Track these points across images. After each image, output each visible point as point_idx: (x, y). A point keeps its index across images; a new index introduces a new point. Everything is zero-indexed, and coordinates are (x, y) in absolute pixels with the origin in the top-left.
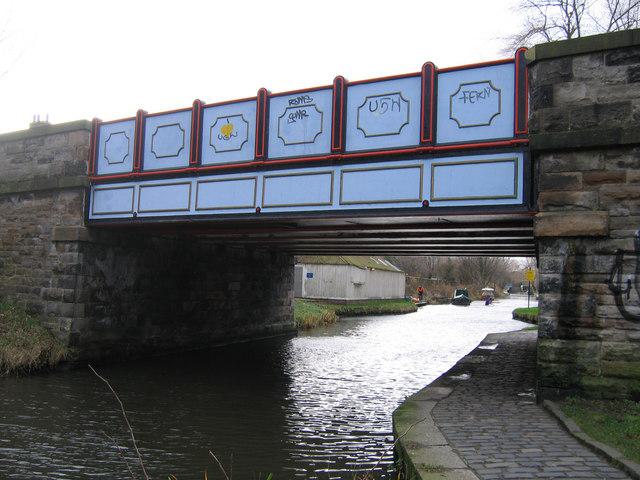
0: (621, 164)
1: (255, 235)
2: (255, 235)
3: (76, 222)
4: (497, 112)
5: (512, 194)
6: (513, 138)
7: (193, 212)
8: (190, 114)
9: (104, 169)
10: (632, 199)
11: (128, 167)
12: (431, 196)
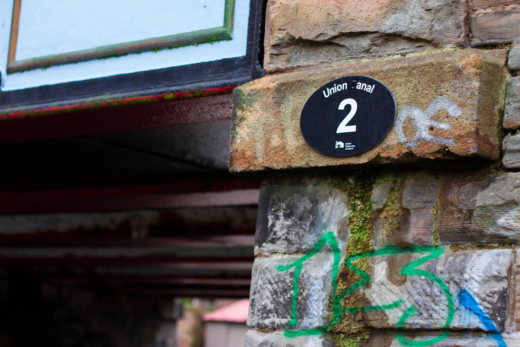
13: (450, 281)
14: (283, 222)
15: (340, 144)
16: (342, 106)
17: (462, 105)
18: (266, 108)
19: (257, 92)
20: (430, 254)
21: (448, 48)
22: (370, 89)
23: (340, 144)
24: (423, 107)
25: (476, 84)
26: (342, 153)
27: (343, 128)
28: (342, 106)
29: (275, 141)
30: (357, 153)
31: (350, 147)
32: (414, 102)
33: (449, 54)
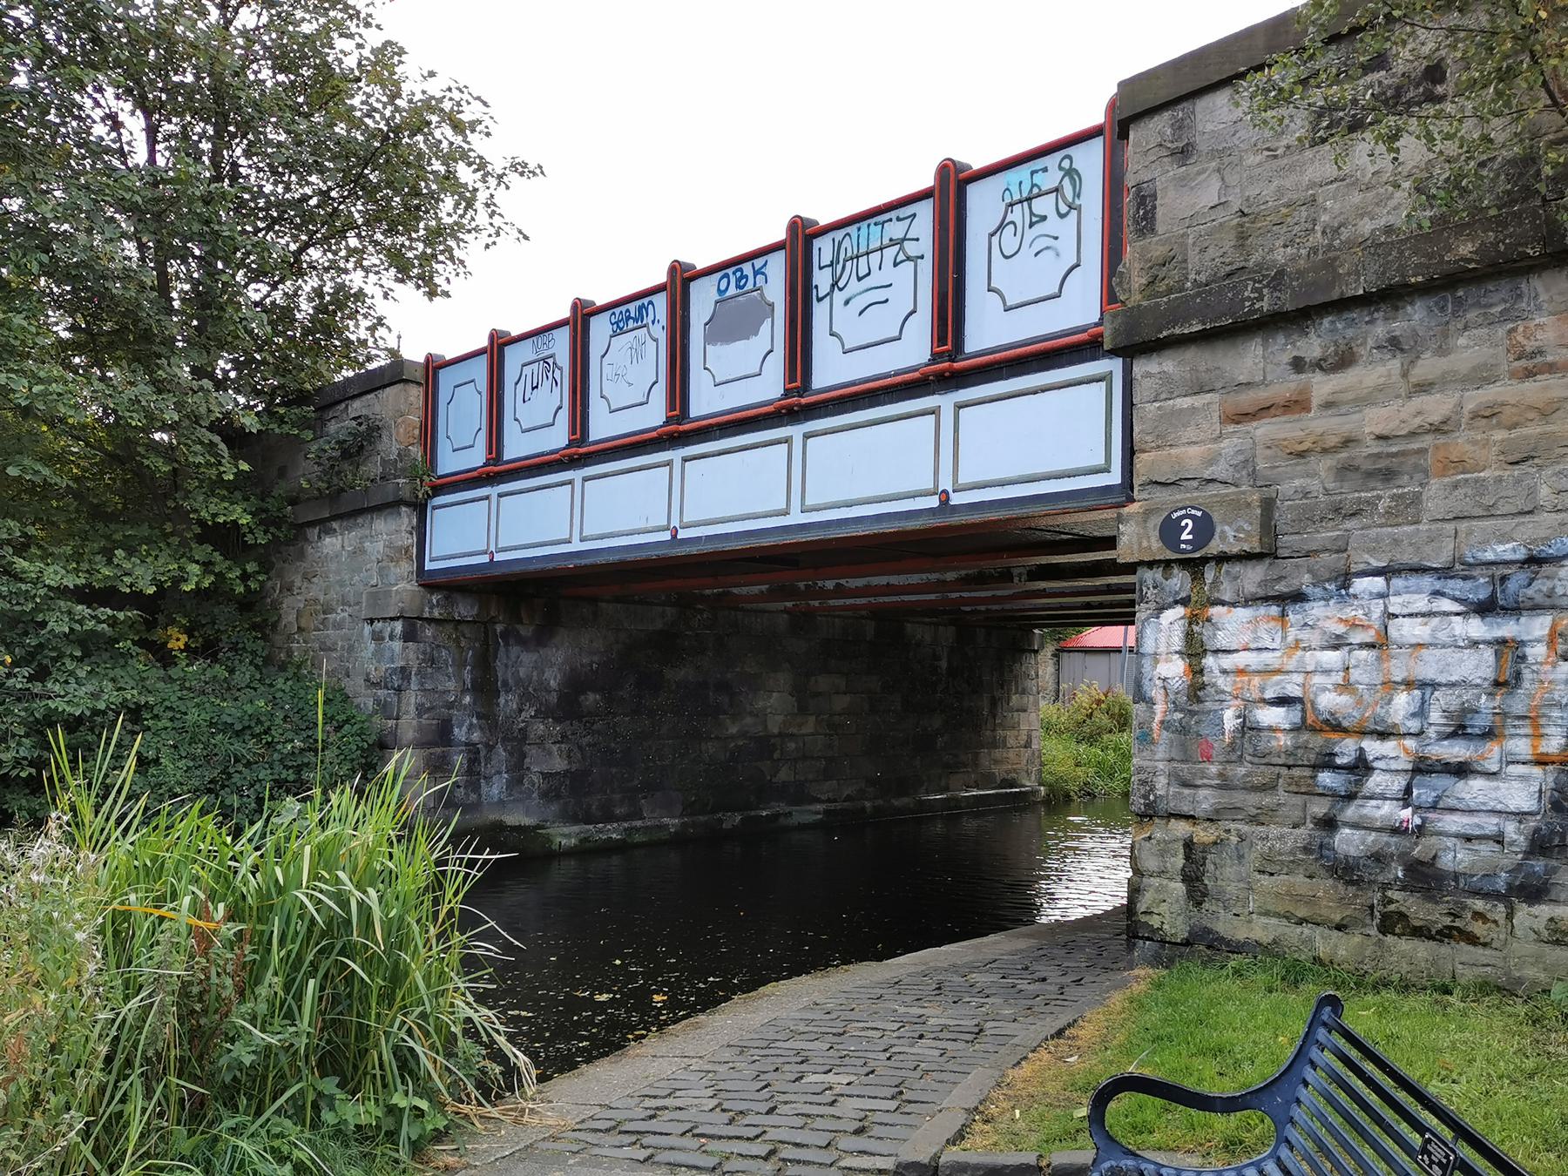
0: (1298, 365)
1: (859, 582)
2: (859, 582)
3: (403, 587)
4: (1075, 261)
5: (1100, 460)
6: (485, 465)
7: (796, 518)
8: (484, 359)
9: (450, 462)
10: (1325, 451)
11: (654, 415)
12: (681, 521)
13: (1189, 610)
14: (479, 185)
15: (1183, 546)
16: (1183, 524)
17: (1251, 524)
18: (1137, 524)
19: (1130, 515)
20: (820, 583)
21: (1244, 488)
22: (1199, 514)
23: (1183, 546)
24: (1230, 524)
25: (1259, 511)
26: (1184, 551)
27: (1185, 536)
28: (1183, 524)
29: (1145, 544)
30: (1193, 551)
31: (1189, 548)
32: (1224, 522)
33: (1244, 493)
